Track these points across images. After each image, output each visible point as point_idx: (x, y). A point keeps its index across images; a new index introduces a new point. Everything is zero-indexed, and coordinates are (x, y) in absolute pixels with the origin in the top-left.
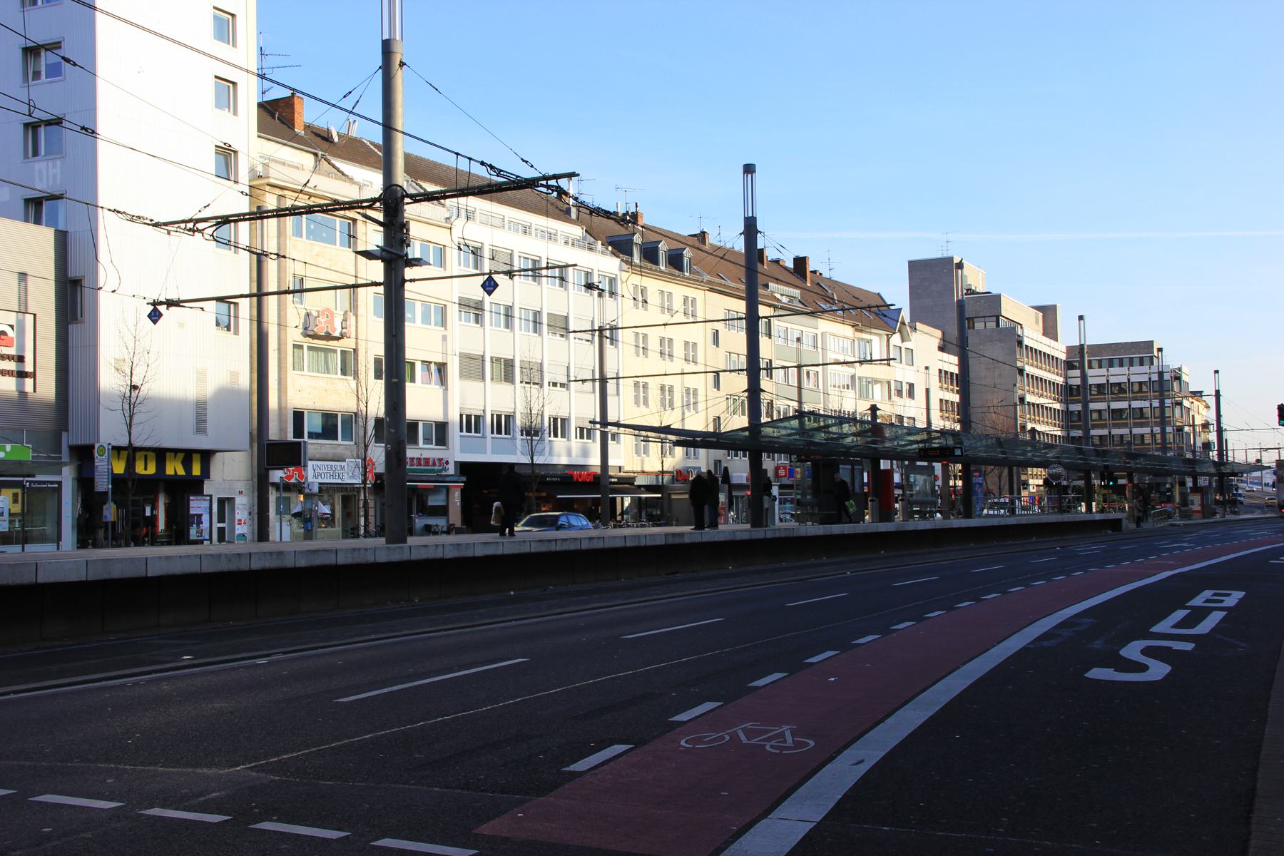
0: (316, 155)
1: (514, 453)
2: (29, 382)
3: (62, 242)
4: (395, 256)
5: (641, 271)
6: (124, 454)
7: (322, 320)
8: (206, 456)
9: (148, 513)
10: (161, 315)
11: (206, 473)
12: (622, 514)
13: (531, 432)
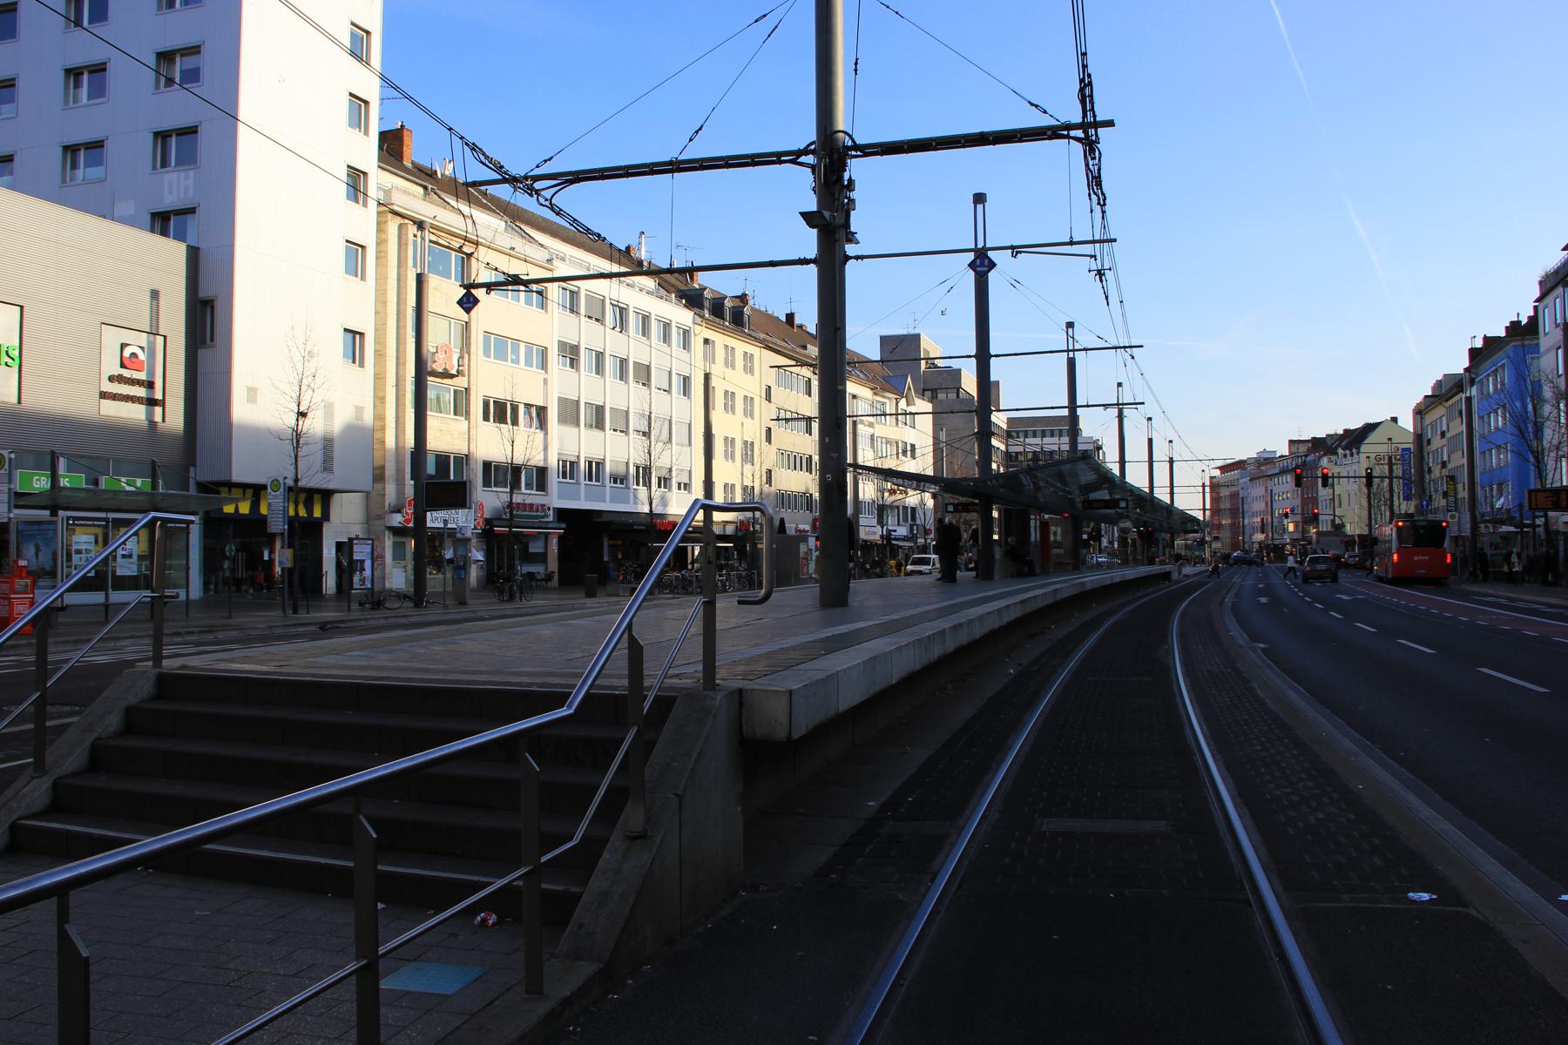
0: (425, 188)
1: (606, 502)
2: (158, 410)
3: (194, 256)
4: (832, 222)
5: (711, 325)
6: (250, 492)
7: (440, 356)
8: (326, 495)
9: (266, 558)
10: (476, 301)
11: (326, 515)
12: (693, 562)
13: (620, 479)
